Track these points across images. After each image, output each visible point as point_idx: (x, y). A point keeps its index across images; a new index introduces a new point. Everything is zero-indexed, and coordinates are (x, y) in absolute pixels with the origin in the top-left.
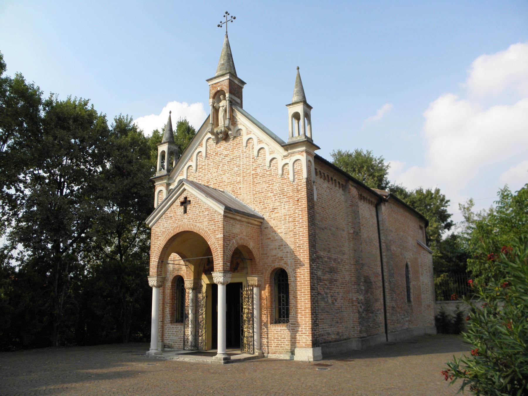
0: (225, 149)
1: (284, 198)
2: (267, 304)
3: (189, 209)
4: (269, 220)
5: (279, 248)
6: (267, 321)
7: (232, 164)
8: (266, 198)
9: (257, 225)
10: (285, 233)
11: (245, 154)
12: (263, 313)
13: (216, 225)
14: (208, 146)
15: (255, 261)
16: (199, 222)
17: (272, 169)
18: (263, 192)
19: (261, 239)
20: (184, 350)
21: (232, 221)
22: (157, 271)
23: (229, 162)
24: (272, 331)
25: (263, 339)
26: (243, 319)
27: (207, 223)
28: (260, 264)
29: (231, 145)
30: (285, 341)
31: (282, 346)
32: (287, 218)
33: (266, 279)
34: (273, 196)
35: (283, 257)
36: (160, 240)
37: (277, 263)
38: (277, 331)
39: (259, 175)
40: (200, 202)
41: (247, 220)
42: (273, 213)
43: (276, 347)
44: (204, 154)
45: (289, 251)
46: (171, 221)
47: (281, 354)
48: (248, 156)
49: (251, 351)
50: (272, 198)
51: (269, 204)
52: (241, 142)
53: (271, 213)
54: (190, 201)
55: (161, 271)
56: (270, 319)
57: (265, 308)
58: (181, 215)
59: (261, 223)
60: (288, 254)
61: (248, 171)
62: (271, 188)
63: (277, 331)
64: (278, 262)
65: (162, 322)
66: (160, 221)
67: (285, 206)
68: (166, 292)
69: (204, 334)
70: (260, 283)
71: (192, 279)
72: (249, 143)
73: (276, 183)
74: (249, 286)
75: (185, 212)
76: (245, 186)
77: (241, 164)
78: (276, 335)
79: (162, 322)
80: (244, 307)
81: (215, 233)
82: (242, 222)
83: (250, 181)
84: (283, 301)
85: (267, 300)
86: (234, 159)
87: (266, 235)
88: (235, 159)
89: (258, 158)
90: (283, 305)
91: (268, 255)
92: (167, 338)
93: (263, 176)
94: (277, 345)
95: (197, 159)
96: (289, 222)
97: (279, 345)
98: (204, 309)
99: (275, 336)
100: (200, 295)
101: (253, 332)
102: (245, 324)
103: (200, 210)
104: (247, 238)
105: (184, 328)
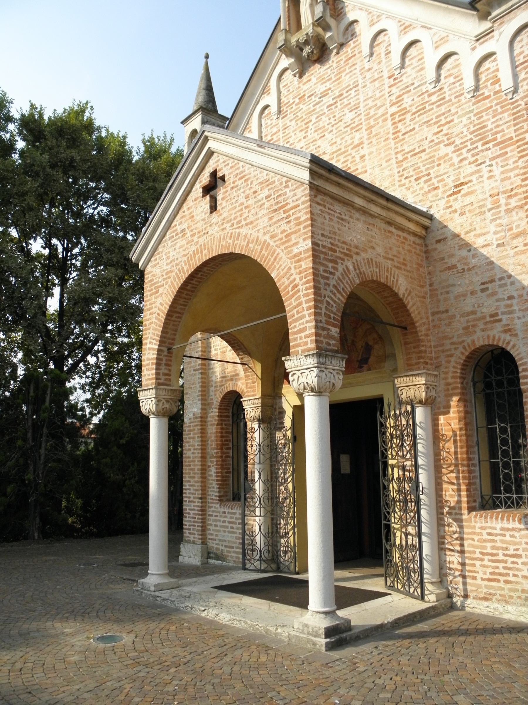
0: (322, 80)
1: (488, 149)
2: (456, 453)
3: (223, 199)
4: (448, 217)
5: (483, 291)
6: (459, 502)
7: (339, 107)
8: (434, 162)
9: (414, 234)
10: (498, 245)
11: (368, 75)
12: (445, 478)
13: (292, 218)
14: (282, 90)
15: (416, 332)
16: (247, 224)
17: (446, 86)
18: (424, 151)
19: (429, 273)
20: (244, 568)
21: (338, 208)
22: (157, 374)
23: (331, 105)
24: (474, 533)
25: (448, 553)
26: (387, 496)
27: (266, 219)
28: (429, 341)
29: (335, 65)
30: (520, 566)
31: (511, 578)
32: (503, 201)
33: (450, 380)
34: (454, 152)
35: (497, 314)
36: (161, 294)
37: (479, 333)
38: (489, 534)
39: (409, 111)
40: (247, 172)
41: (384, 213)
42: (459, 195)
43: (489, 580)
44: (274, 108)
45: (515, 294)
46: (184, 242)
47: (506, 602)
48: (376, 76)
49: (416, 589)
50: (451, 158)
51: (445, 177)
52: (356, 52)
53: (451, 198)
54: (223, 178)
55: (169, 375)
56: (468, 496)
57: (450, 465)
58: (204, 220)
59: (426, 228)
60: (514, 302)
61: (381, 111)
62: (447, 134)
63: (489, 534)
64: (483, 330)
65: (201, 498)
66: (160, 249)
67: (491, 171)
68: (209, 431)
69: (291, 533)
70: (433, 393)
71: (259, 395)
72: (378, 45)
73: (459, 117)
74: (401, 403)
75: (214, 208)
76: (374, 149)
77: (362, 100)
78: (489, 545)
79: (201, 498)
80: (390, 462)
81: (288, 241)
82: (372, 216)
83: (388, 134)
84: (504, 442)
85: (455, 442)
86: (342, 95)
87: (443, 259)
88: (345, 95)
89: (403, 71)
90: (505, 454)
91: (450, 313)
92: (214, 537)
93: (421, 110)
94: (491, 573)
95: (260, 126)
96: (508, 211)
97: (500, 574)
98: (290, 469)
99: (485, 548)
100: (279, 435)
101: (419, 534)
102: (394, 511)
103: (248, 192)
104: (389, 263)
105: (244, 515)
